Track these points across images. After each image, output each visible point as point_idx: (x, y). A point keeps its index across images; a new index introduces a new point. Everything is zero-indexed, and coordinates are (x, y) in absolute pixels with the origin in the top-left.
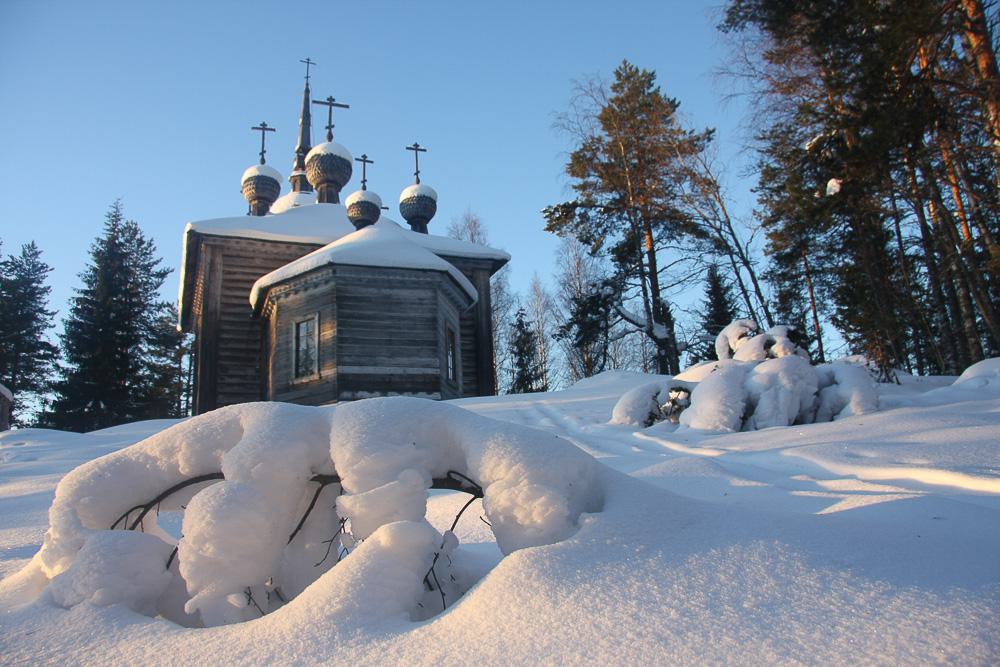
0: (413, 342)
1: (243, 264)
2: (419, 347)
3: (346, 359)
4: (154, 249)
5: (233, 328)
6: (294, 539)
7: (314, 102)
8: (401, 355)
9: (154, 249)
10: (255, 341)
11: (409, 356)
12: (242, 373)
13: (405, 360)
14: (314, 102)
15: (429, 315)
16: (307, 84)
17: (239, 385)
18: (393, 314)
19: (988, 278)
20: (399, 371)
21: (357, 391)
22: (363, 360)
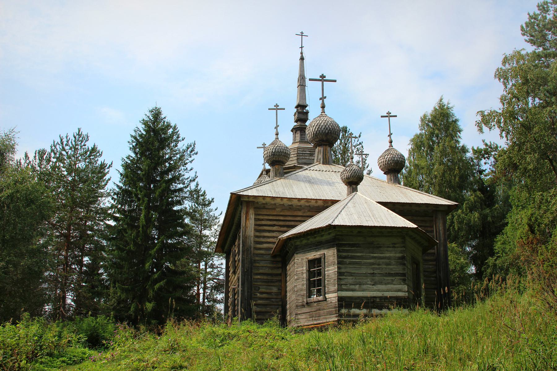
0: (390, 275)
1: (268, 213)
3: (344, 287)
6: (296, 84)
7: (310, 80)
8: (381, 283)
12: (268, 291)
14: (310, 80)
16: (302, 53)
17: (267, 299)
18: (375, 255)
19: (155, 270)
22: (352, 287)
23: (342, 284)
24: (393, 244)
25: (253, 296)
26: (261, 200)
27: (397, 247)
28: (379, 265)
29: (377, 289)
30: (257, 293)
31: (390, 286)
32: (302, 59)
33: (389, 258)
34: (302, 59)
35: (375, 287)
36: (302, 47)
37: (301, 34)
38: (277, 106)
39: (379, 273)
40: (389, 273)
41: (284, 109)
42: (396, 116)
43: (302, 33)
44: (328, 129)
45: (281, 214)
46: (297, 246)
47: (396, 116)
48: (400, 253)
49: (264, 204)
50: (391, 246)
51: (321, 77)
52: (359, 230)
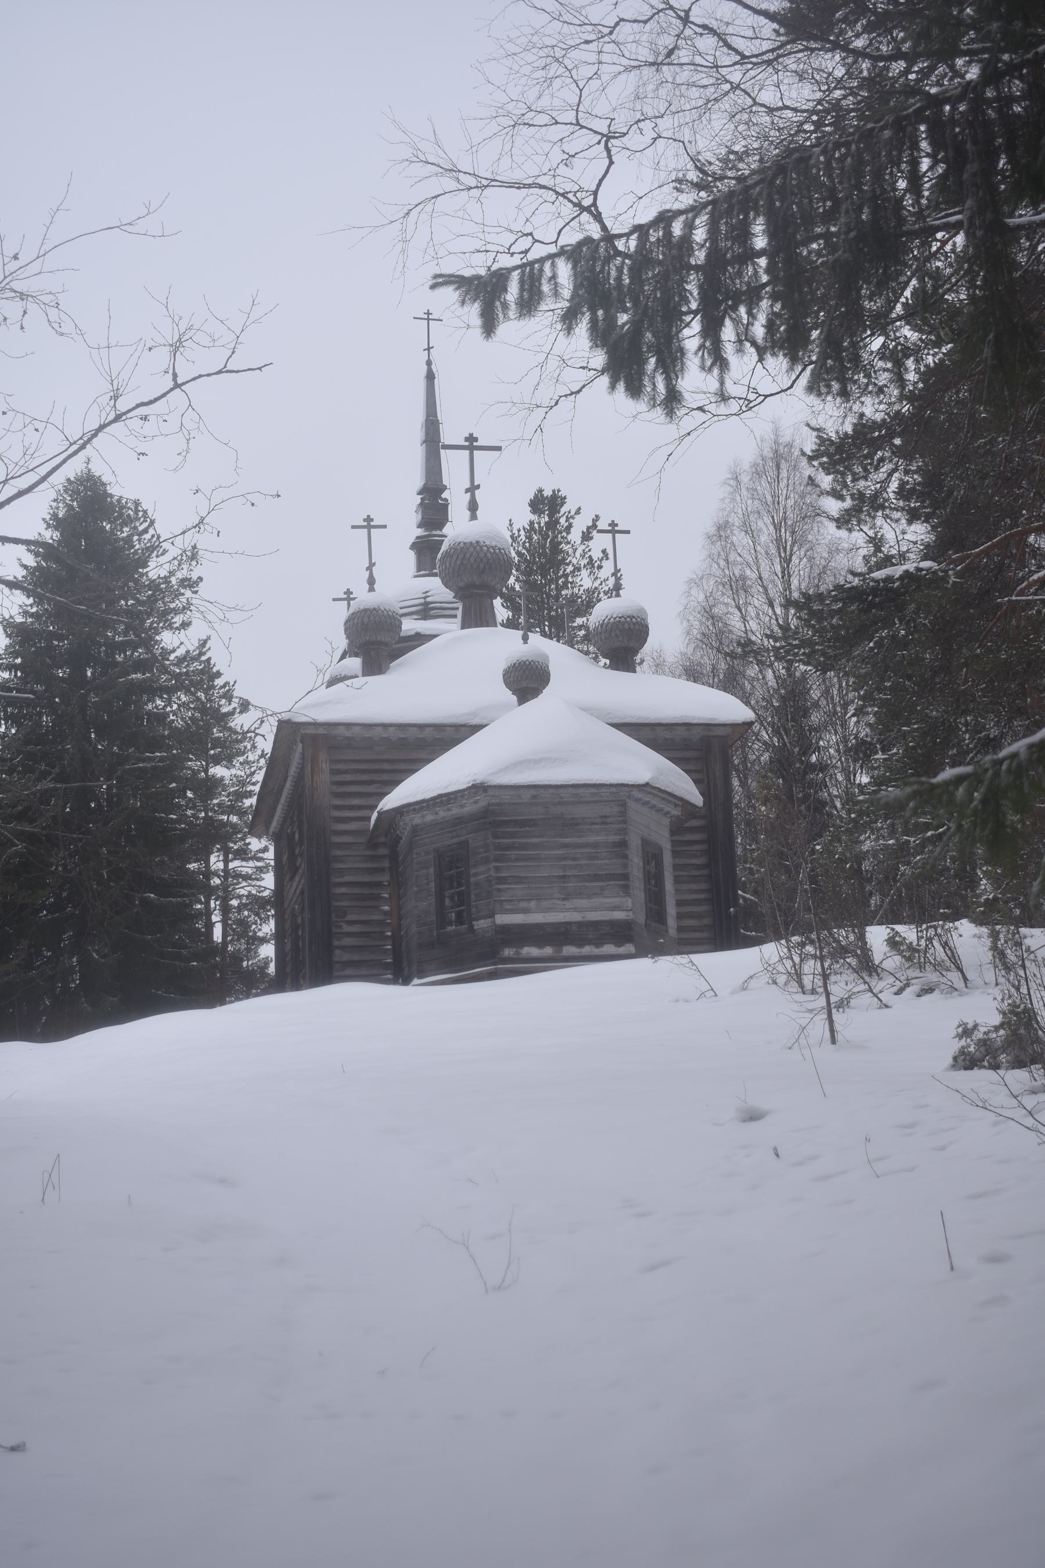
0: (597, 878)
2: (605, 884)
4: (209, 649)
5: (356, 957)
6: (418, 434)
9: (209, 649)
10: (382, 870)
11: (589, 897)
13: (584, 903)
15: (616, 838)
16: (429, 363)
17: (361, 934)
20: (576, 917)
21: (522, 947)
23: (504, 901)
24: (601, 817)
25: (334, 930)
26: (342, 730)
27: (611, 823)
28: (574, 859)
29: (571, 906)
30: (341, 924)
31: (596, 901)
32: (430, 377)
33: (595, 845)
34: (430, 377)
35: (568, 904)
36: (429, 349)
37: (426, 316)
38: (369, 519)
39: (575, 876)
40: (595, 875)
41: (385, 527)
42: (628, 532)
43: (428, 313)
44: (485, 560)
45: (385, 757)
46: (417, 826)
47: (628, 532)
48: (615, 834)
49: (348, 738)
50: (599, 820)
51: (467, 439)
52: (533, 792)
